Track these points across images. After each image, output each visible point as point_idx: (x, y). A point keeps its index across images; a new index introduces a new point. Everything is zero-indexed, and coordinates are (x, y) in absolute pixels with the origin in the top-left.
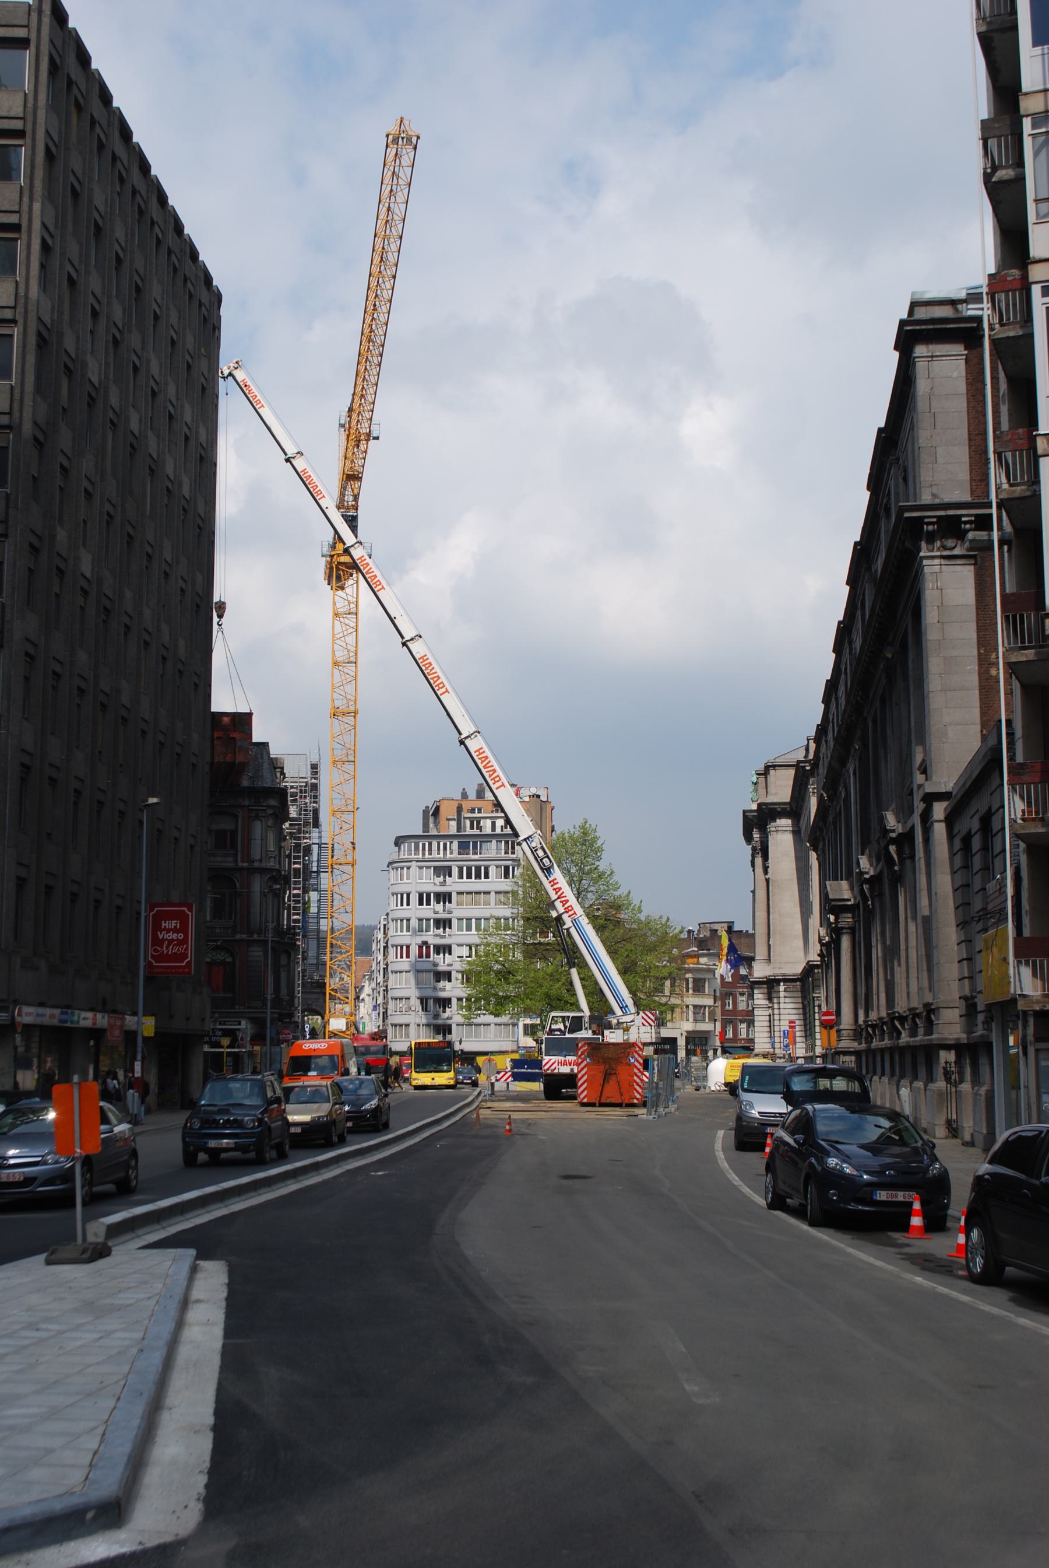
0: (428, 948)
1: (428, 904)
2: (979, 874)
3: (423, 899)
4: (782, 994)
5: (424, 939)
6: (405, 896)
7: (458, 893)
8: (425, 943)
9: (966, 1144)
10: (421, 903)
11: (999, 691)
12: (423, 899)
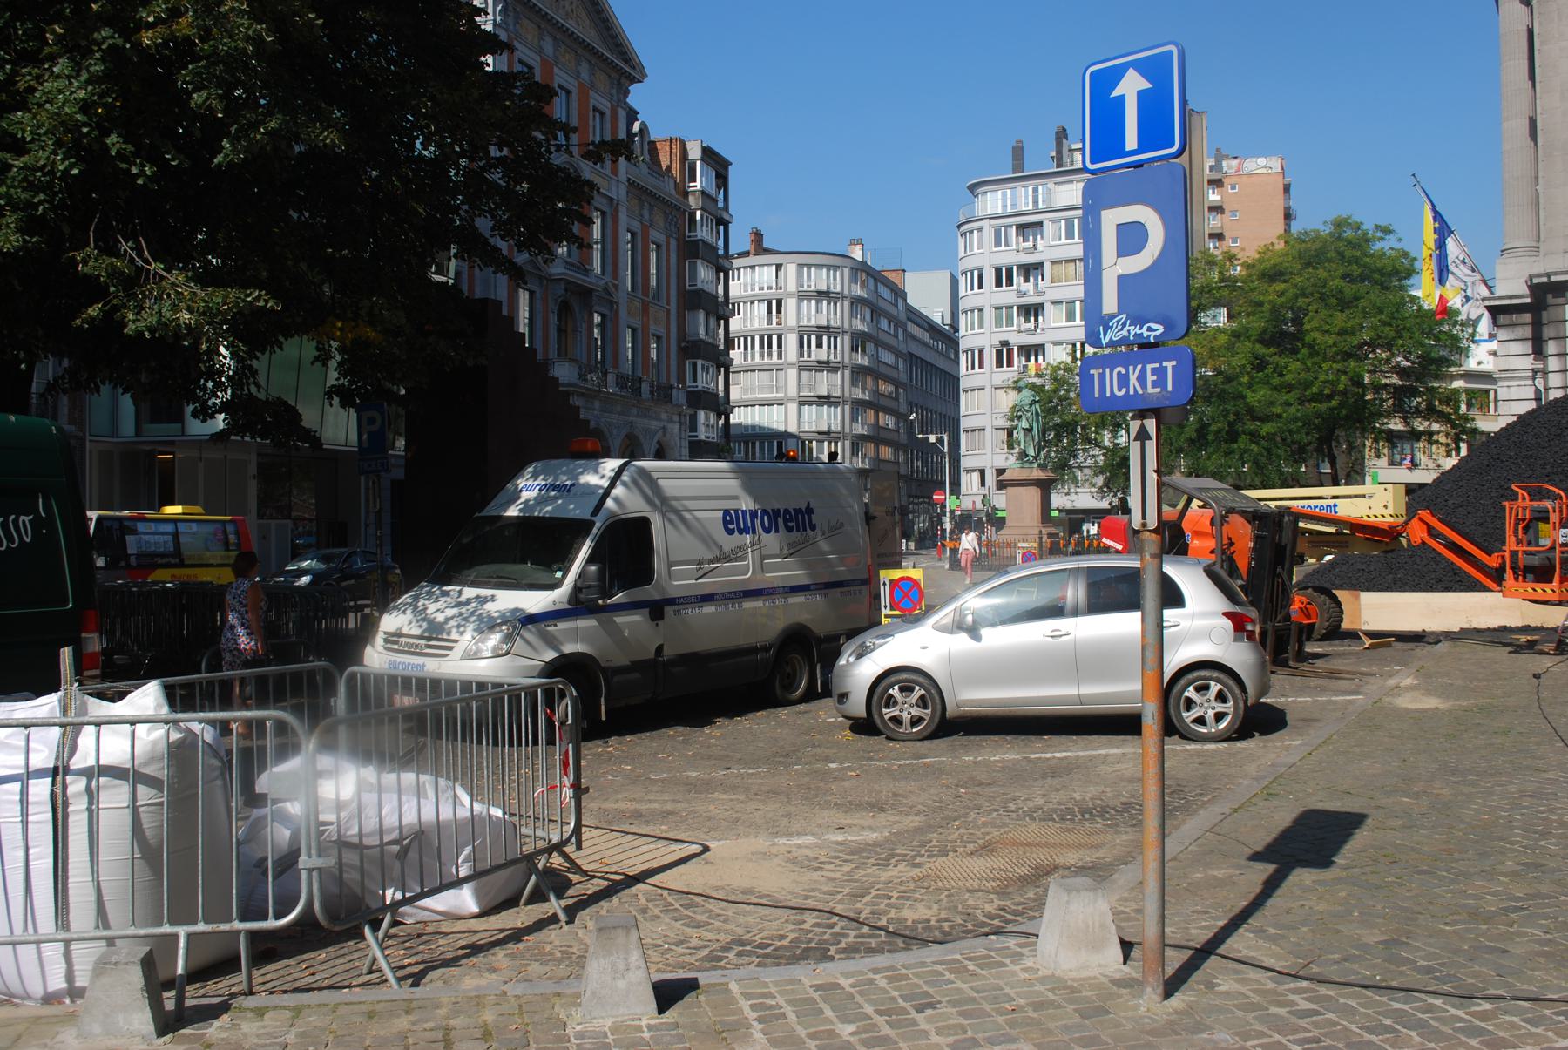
0: (1010, 351)
1: (1010, 283)
3: (1004, 276)
5: (1004, 337)
7: (1054, 262)
8: (1005, 343)
9: (865, 726)
10: (999, 284)
11: (275, 903)
12: (1004, 276)
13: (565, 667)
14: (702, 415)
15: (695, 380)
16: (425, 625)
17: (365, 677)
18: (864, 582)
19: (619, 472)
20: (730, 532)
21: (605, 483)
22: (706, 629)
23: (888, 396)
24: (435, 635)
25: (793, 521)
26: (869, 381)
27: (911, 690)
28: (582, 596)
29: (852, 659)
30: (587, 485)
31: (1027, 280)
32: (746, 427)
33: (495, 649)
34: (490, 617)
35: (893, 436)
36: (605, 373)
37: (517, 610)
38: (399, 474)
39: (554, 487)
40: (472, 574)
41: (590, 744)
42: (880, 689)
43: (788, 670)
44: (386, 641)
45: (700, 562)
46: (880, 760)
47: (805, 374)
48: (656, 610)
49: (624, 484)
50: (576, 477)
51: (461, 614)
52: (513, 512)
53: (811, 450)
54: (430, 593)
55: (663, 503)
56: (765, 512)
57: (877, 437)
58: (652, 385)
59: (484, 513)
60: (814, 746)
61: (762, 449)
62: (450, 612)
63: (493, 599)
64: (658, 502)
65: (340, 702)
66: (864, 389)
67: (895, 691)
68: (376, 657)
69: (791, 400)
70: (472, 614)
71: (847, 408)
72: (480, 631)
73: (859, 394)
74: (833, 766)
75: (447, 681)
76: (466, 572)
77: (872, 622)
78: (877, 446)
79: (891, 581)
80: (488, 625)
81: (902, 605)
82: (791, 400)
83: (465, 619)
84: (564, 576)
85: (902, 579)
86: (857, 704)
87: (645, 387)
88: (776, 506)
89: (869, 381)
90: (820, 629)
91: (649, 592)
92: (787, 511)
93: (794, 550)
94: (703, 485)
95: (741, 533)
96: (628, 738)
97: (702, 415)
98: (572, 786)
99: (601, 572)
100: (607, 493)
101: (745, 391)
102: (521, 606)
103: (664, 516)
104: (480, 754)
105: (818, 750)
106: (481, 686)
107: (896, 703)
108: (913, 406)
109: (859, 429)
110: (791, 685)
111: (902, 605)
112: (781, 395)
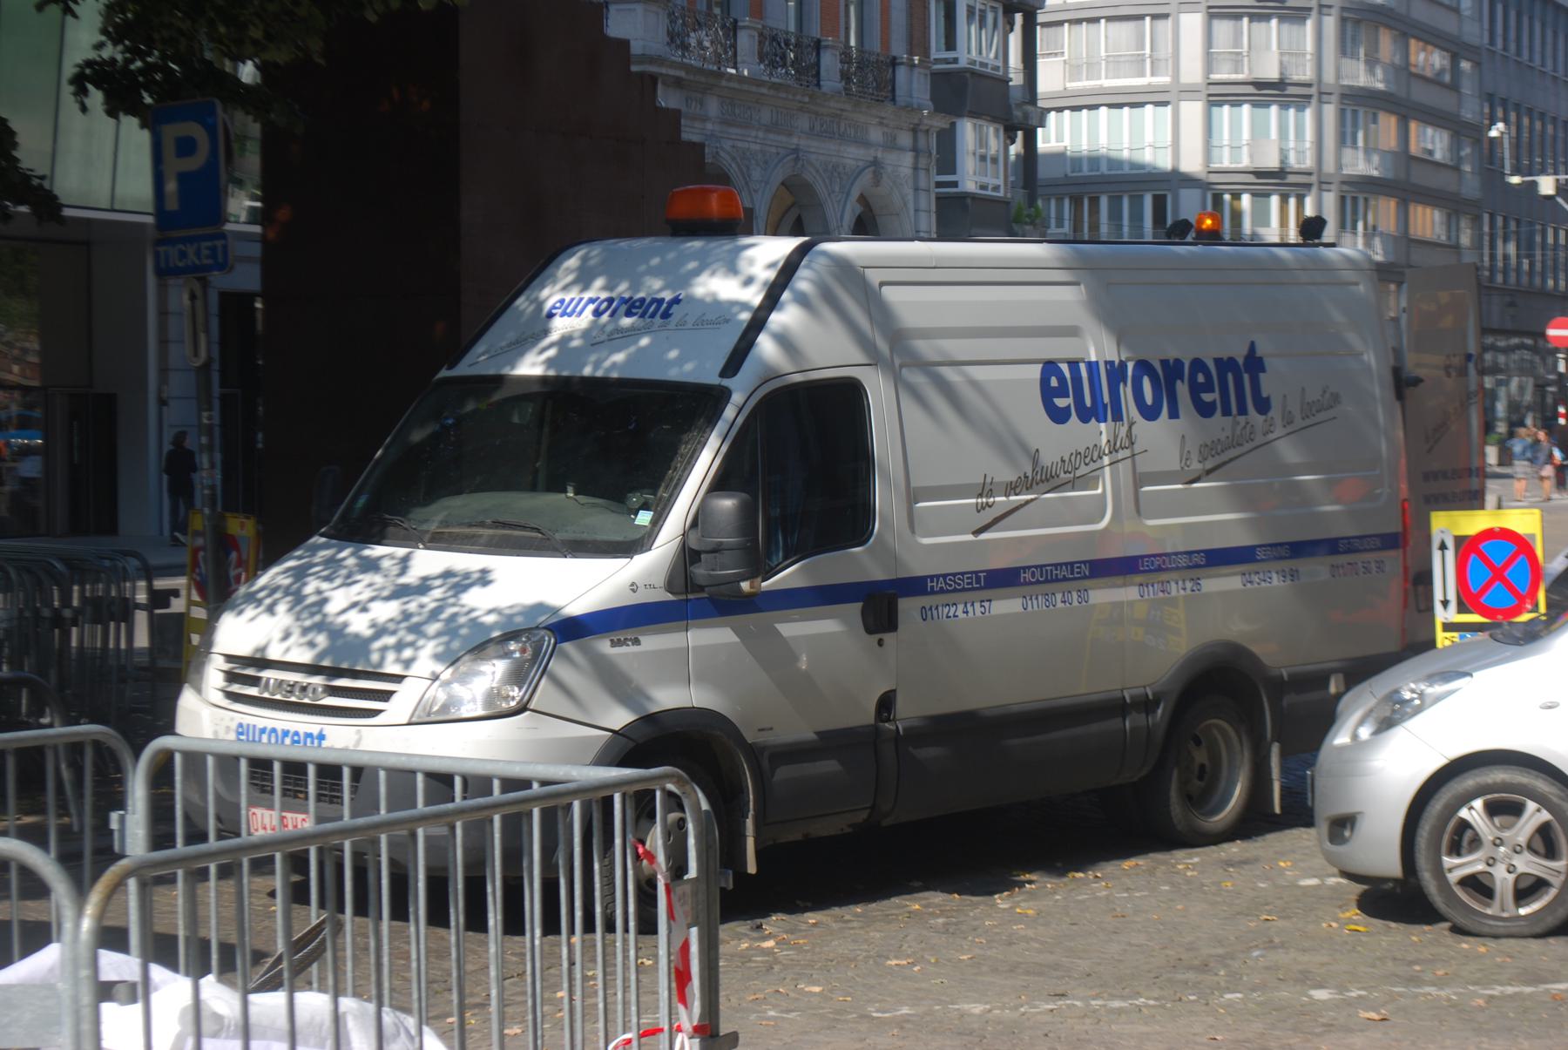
9: (1398, 900)
13: (655, 741)
14: (967, 131)
15: (950, 44)
16: (322, 640)
17: (195, 760)
18: (1392, 541)
19: (788, 270)
20: (1059, 416)
21: (754, 296)
22: (995, 656)
23: (1435, 81)
24: (349, 675)
25: (1214, 388)
26: (1386, 44)
27: (1516, 810)
28: (700, 571)
29: (1365, 733)
30: (717, 304)
32: (1077, 161)
33: (492, 697)
34: (474, 623)
35: (1443, 181)
36: (733, 29)
37: (540, 608)
38: (247, 278)
39: (631, 306)
40: (435, 515)
41: (726, 926)
42: (1437, 806)
43: (1200, 756)
44: (231, 677)
45: (986, 489)
46: (1439, 983)
47: (1223, 28)
48: (880, 606)
49: (802, 300)
50: (687, 279)
51: (406, 616)
52: (531, 366)
53: (1237, 216)
54: (332, 563)
55: (894, 345)
56: (1144, 366)
57: (1405, 184)
58: (846, 56)
59: (463, 369)
60: (1270, 945)
61: (1115, 215)
62: (386, 611)
63: (484, 578)
64: (883, 346)
65: (133, 826)
66: (1371, 62)
67: (1474, 813)
68: (205, 716)
69: (1189, 92)
70: (434, 615)
71: (1330, 111)
72: (450, 658)
73: (1360, 76)
74: (1321, 995)
75: (392, 771)
76: (418, 513)
77: (1415, 643)
78: (1404, 205)
79: (1459, 540)
80: (473, 644)
81: (1486, 600)
82: (1189, 92)
83: (416, 629)
84: (657, 522)
85: (1489, 534)
86: (1377, 844)
87: (830, 63)
88: (1172, 354)
89: (1386, 42)
90: (1275, 655)
91: (858, 563)
92: (1198, 365)
93: (1215, 461)
94: (989, 307)
95: (1084, 418)
96: (811, 918)
97: (967, 131)
98: (698, 1030)
99: (747, 514)
100: (758, 322)
101: (1073, 70)
102: (553, 600)
103: (898, 382)
104: (401, 955)
105: (1279, 957)
106: (478, 784)
107: (1476, 842)
108: (1496, 104)
109: (1360, 164)
110: (1204, 794)
111: (1486, 600)
112: (1164, 80)
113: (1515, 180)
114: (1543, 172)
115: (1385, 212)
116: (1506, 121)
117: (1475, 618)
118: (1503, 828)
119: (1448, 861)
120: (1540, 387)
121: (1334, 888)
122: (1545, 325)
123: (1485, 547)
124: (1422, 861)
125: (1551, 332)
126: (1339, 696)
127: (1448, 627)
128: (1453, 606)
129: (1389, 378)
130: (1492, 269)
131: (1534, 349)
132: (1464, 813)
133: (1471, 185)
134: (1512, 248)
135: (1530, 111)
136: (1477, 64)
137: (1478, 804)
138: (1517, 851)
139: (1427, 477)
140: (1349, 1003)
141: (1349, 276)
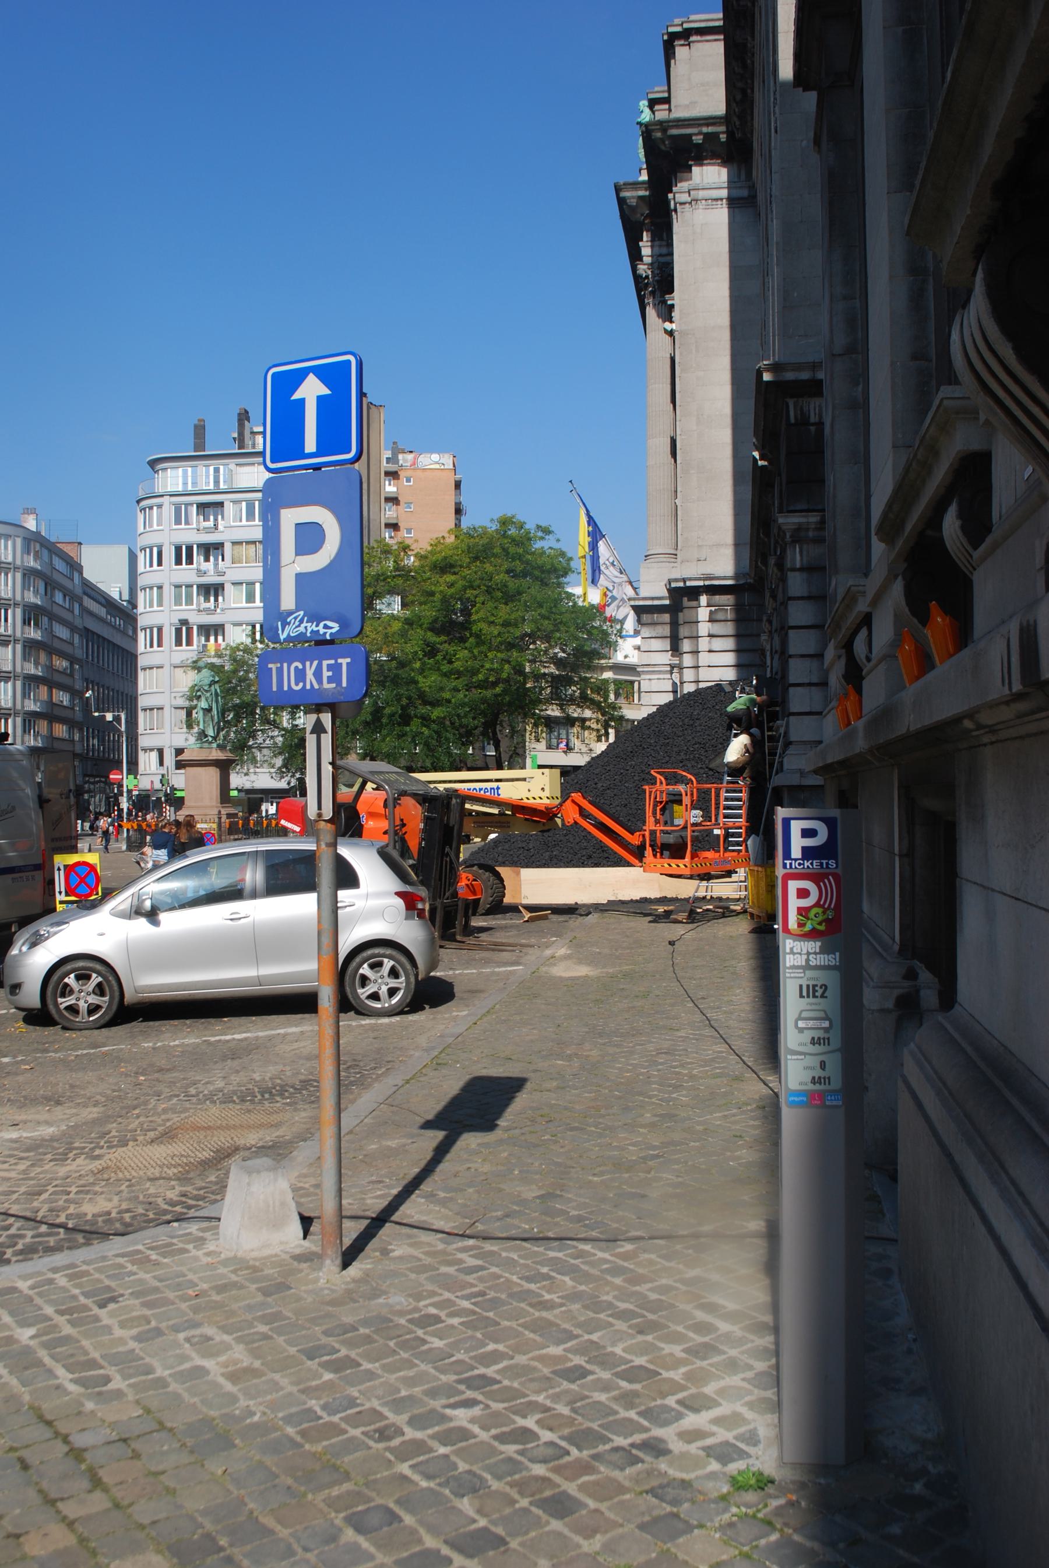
1: (190, 561)
2: (883, 667)
3: (183, 554)
4: (704, 628)
5: (184, 616)
6: (155, 550)
8: (184, 622)
9: (40, 1017)
10: (178, 562)
12: (183, 554)
18: (37, 867)
23: (63, 673)
26: (43, 657)
27: (88, 977)
29: (24, 949)
31: (207, 560)
35: (68, 714)
42: (55, 978)
46: (56, 1051)
57: (51, 714)
66: (37, 664)
67: (71, 980)
71: (19, 684)
73: (31, 669)
74: (6, 1060)
78: (50, 723)
79: (66, 866)
81: (78, 891)
85: (78, 864)
86: (31, 995)
107: (72, 992)
108: (89, 683)
109: (31, 706)
111: (78, 891)
113: (96, 714)
114: (108, 711)
115: (43, 726)
116: (93, 691)
117: (73, 898)
118: (83, 985)
119: (60, 1000)
120: (108, 798)
121: (13, 1014)
122: (109, 772)
123: (77, 869)
124: (49, 1001)
125: (111, 776)
126: (15, 932)
127: (61, 902)
128: (63, 893)
129: (36, 799)
130: (88, 750)
131: (106, 783)
132: (66, 980)
133: (78, 715)
134: (96, 742)
135: (103, 686)
136: (81, 666)
137: (72, 976)
138: (88, 994)
139: (53, 840)
140: (17, 1063)
141: (19, 757)
